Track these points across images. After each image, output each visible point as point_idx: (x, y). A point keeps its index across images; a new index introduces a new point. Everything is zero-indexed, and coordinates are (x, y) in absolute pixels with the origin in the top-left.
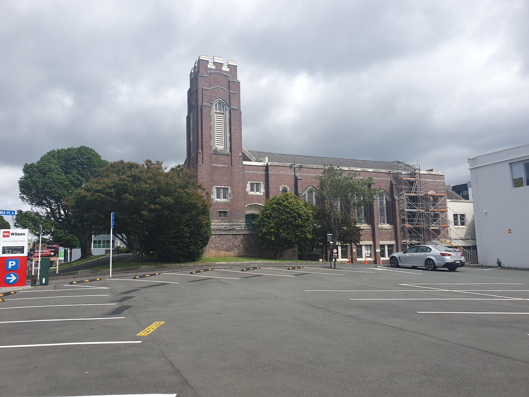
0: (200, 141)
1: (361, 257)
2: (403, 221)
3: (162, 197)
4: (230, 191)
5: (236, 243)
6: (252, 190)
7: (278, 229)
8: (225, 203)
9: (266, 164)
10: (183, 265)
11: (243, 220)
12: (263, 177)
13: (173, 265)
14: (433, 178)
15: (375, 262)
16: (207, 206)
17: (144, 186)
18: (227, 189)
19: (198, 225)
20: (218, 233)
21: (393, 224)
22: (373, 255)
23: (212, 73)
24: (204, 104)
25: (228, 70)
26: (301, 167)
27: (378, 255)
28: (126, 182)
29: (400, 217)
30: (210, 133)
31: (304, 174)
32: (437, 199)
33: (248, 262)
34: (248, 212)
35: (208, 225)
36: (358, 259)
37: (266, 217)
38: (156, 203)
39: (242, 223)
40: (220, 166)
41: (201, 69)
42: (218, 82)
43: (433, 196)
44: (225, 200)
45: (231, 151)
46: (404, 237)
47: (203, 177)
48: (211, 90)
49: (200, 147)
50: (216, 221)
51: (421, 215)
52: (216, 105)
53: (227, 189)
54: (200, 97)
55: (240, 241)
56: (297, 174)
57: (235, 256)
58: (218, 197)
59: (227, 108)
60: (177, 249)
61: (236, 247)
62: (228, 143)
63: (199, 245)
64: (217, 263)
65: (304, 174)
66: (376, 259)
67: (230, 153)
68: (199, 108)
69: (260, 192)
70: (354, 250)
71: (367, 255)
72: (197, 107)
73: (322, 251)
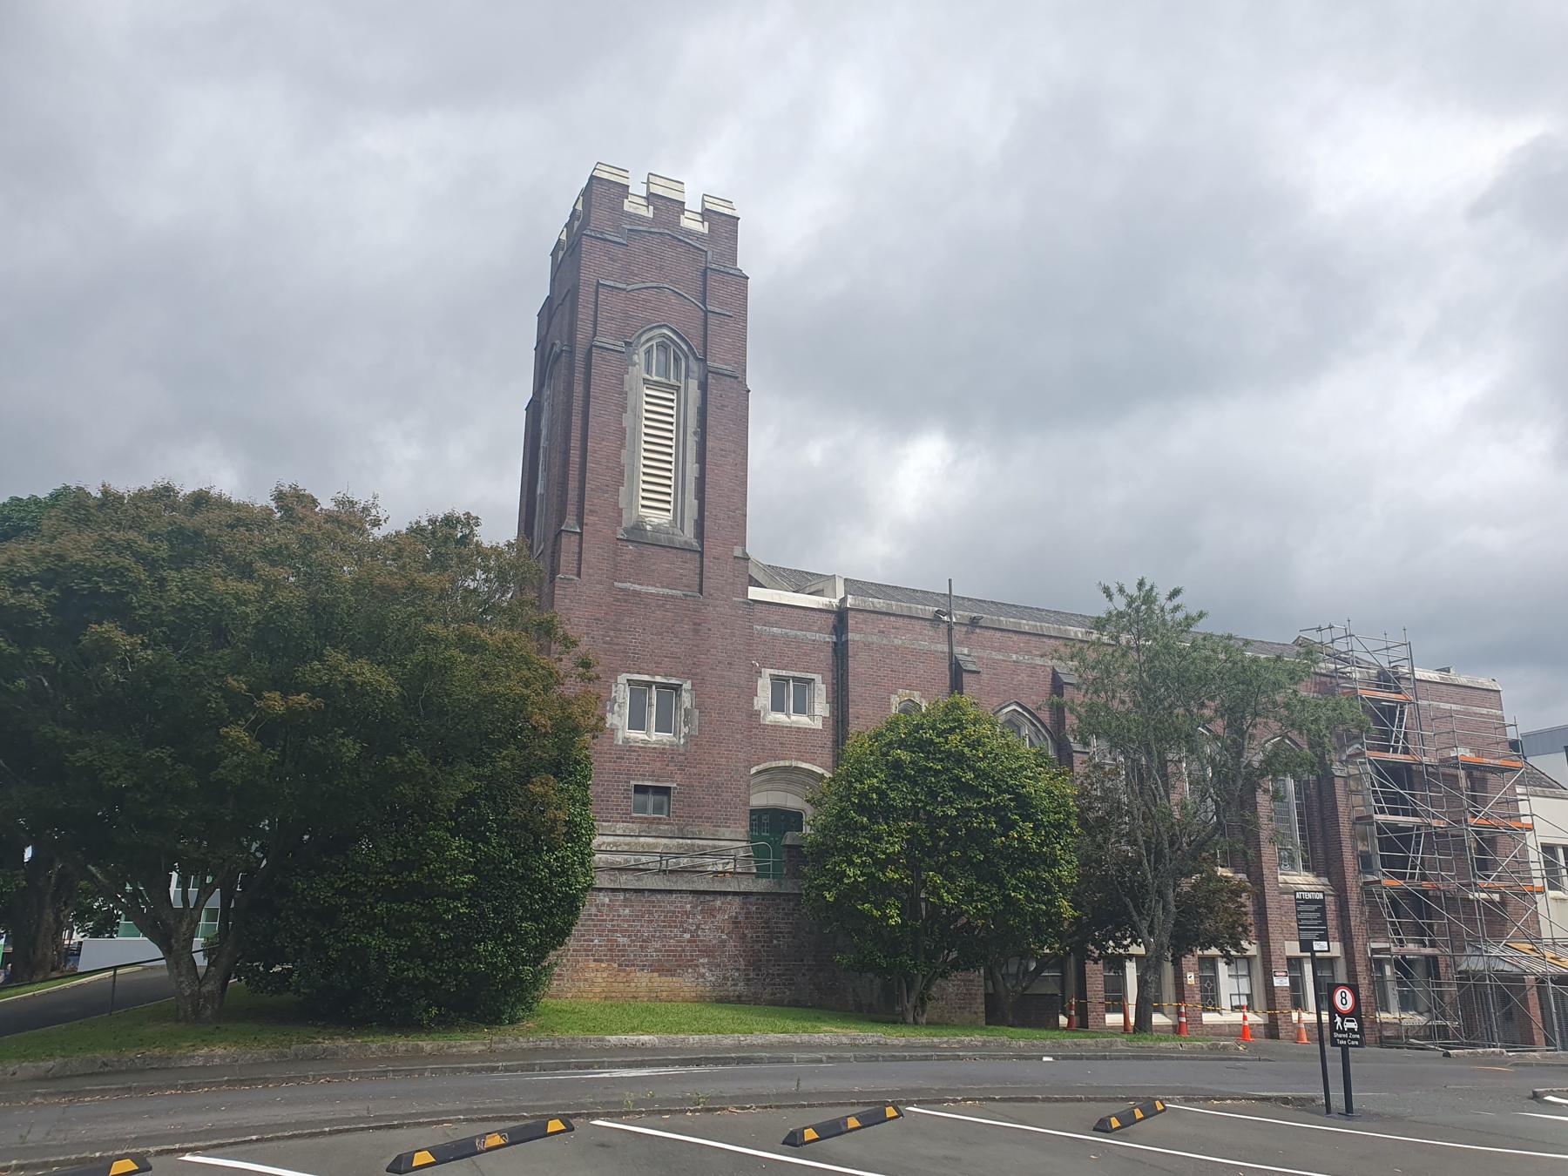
0: (573, 484)
1: (1216, 1008)
2: (1365, 863)
3: (336, 656)
4: (687, 700)
5: (709, 935)
6: (778, 706)
7: (914, 867)
8: (663, 752)
9: (836, 602)
10: (427, 1045)
11: (741, 829)
12: (826, 656)
13: (376, 1044)
14: (1463, 701)
15: (1272, 1030)
16: (576, 730)
17: (225, 586)
18: (677, 688)
19: (524, 826)
20: (627, 881)
21: (1327, 874)
22: (1260, 1000)
23: (636, 230)
24: (601, 340)
25: (704, 229)
26: (974, 622)
27: (1284, 1000)
28: (128, 561)
29: (1354, 848)
30: (616, 504)
31: (985, 654)
32: (1484, 780)
33: (773, 1037)
34: (760, 800)
35: (578, 833)
36: (1208, 1018)
37: (861, 809)
38: (287, 687)
39: (734, 839)
40: (652, 590)
41: (599, 216)
42: (661, 268)
43: (1469, 768)
44: (666, 737)
45: (700, 533)
46: (1376, 929)
47: (578, 608)
48: (633, 303)
49: (572, 508)
50: (620, 827)
51: (1438, 840)
52: (648, 352)
53: (677, 688)
54: (585, 313)
55: (728, 927)
56: (961, 651)
57: (700, 999)
58: (637, 722)
59: (694, 366)
60: (401, 955)
61: (707, 952)
62: (691, 502)
63: (521, 940)
64: (613, 1039)
65: (985, 654)
66: (1273, 1019)
67: (695, 543)
68: (580, 356)
69: (812, 716)
70: (1191, 979)
71: (1236, 1003)
72: (572, 352)
73: (1063, 978)
